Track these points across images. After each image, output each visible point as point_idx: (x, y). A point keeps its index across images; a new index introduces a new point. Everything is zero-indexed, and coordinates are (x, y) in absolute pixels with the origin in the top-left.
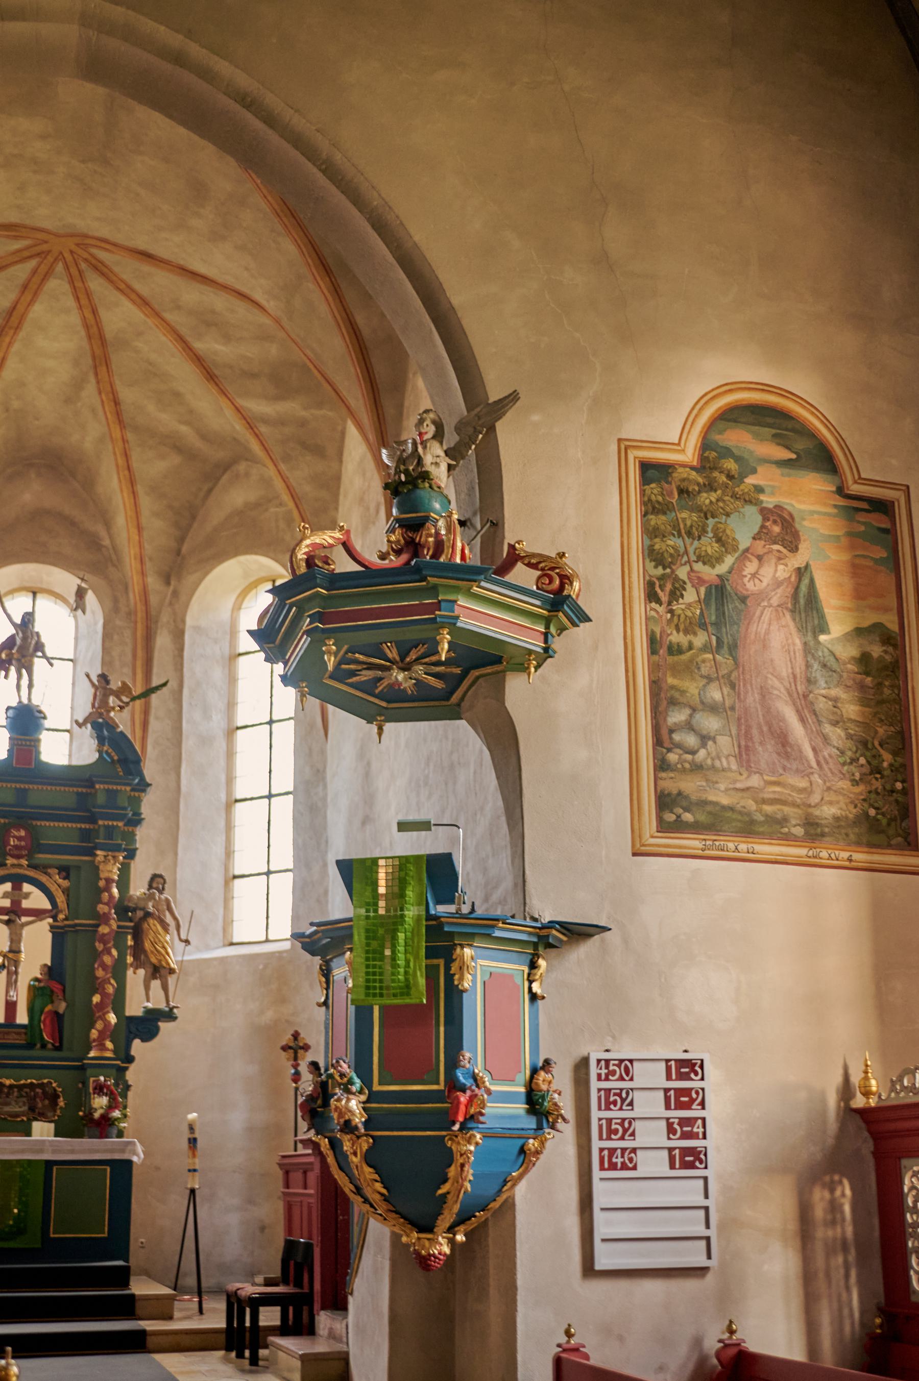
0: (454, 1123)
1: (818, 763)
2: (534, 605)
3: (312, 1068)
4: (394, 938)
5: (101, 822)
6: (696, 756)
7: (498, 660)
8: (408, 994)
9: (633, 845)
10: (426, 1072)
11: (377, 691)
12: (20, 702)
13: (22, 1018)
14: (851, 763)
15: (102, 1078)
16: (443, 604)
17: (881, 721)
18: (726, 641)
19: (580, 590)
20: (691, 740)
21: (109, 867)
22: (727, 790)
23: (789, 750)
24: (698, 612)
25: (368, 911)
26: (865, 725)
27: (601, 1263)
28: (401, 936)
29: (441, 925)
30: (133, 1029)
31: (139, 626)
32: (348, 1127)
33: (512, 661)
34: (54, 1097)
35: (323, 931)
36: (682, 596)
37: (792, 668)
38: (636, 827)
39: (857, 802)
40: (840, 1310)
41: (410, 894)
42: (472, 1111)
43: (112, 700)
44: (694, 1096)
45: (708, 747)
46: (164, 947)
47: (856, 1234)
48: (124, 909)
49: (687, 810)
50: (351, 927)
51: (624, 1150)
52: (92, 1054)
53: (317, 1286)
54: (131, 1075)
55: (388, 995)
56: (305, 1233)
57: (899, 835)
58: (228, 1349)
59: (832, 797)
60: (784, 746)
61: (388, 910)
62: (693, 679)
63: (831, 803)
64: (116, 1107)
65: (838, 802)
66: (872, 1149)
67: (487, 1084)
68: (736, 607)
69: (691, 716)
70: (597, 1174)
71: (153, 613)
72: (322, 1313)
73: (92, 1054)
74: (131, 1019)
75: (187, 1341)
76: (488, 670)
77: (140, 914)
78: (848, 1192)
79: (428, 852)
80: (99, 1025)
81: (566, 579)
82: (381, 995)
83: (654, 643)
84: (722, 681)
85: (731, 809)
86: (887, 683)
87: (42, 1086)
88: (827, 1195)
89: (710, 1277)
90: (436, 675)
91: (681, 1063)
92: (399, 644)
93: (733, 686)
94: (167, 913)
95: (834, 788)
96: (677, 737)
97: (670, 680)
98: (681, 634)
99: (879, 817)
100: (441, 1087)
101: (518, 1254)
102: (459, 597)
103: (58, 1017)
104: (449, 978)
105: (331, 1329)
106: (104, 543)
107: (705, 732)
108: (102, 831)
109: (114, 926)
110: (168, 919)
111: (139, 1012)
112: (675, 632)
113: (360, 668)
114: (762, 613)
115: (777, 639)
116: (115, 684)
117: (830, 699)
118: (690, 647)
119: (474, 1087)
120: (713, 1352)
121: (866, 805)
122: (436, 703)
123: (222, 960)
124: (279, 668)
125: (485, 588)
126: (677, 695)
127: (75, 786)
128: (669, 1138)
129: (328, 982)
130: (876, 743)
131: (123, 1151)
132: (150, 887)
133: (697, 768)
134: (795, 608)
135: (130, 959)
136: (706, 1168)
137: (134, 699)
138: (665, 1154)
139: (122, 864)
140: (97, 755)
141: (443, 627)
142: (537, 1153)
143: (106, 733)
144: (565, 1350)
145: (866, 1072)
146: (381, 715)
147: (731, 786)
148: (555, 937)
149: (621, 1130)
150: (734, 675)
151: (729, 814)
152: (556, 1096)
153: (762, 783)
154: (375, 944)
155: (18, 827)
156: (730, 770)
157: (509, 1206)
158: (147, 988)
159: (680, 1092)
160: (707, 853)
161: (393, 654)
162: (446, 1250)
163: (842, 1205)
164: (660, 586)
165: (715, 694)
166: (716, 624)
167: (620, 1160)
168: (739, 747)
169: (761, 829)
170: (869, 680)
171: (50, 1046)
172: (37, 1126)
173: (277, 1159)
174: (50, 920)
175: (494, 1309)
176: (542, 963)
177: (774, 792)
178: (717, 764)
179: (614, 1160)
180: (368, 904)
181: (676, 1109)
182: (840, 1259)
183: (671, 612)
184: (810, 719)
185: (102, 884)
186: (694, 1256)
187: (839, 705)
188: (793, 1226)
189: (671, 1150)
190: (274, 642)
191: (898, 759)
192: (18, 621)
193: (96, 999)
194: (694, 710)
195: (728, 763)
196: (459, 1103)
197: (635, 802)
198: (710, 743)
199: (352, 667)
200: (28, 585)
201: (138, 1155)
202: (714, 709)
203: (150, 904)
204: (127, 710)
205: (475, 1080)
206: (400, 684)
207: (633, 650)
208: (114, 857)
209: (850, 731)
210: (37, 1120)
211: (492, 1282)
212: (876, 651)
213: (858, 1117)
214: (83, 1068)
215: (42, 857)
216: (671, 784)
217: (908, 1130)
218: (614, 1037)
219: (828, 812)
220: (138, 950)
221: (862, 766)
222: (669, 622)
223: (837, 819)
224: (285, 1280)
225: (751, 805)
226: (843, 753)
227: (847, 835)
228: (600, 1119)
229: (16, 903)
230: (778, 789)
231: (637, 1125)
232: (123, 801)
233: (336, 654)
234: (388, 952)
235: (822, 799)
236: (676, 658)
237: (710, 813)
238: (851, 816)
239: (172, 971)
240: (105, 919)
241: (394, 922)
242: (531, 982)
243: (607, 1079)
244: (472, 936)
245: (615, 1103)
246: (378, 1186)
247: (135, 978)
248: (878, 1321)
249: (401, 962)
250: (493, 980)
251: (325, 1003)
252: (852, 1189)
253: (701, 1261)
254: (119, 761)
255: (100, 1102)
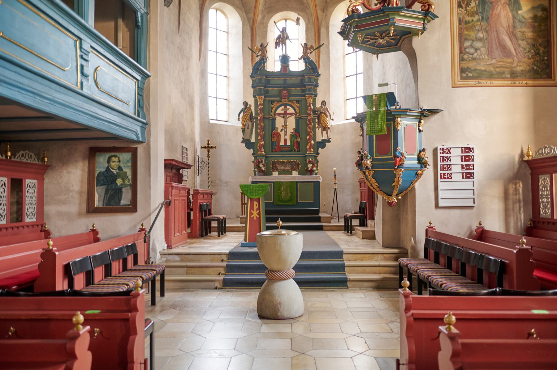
0: (396, 167)
1: (516, 53)
2: (419, 15)
3: (359, 153)
4: (378, 116)
5: (307, 87)
6: (473, 56)
7: (410, 33)
8: (382, 132)
9: (452, 84)
10: (387, 152)
11: (375, 45)
12: (283, 54)
13: (289, 143)
14: (528, 52)
15: (310, 159)
16: (391, 19)
17: (540, 37)
18: (485, 17)
19: (434, 8)
20: (472, 51)
21: (310, 100)
22: (484, 65)
23: (506, 50)
24: (475, 9)
25: (370, 110)
26: (534, 40)
27: (440, 205)
28: (380, 116)
29: (391, 112)
30: (319, 146)
31: (316, 26)
32: (367, 168)
33: (414, 33)
34: (298, 164)
35: (359, 116)
36: (470, 5)
37: (508, 23)
38: (453, 79)
39: (530, 65)
40: (517, 219)
41: (382, 104)
42: (401, 163)
43: (308, 51)
44: (470, 158)
45: (478, 52)
46: (326, 122)
47: (523, 198)
48: (315, 112)
49: (470, 72)
50: (366, 114)
51: (448, 173)
52: (308, 153)
53: (368, 214)
54: (319, 158)
55: (376, 132)
56: (365, 200)
57: (545, 74)
58: (345, 231)
59: (521, 64)
60: (504, 49)
61: (376, 109)
62: (473, 31)
63: (520, 66)
64: (314, 167)
65: (523, 65)
66: (530, 172)
67: (405, 155)
68: (489, 6)
69: (472, 43)
70: (439, 180)
71: (320, 22)
72: (369, 220)
73: (308, 153)
74: (318, 142)
75: (334, 228)
76: (407, 36)
77: (319, 112)
78: (521, 185)
79: (387, 92)
80: (309, 144)
81: (430, 6)
82: (374, 132)
83: (460, 21)
84: (483, 31)
85: (485, 71)
86: (543, 24)
87: (295, 162)
88: (514, 186)
89: (474, 209)
90: (392, 39)
91: (466, 148)
92: (379, 32)
93: (487, 32)
94: (327, 112)
95: (522, 61)
96: (467, 50)
97: (465, 32)
98: (469, 17)
99: (538, 69)
100: (392, 157)
101: (416, 202)
102: (396, 16)
103: (298, 143)
104: (394, 127)
105: (371, 225)
106: (304, 2)
107: (476, 48)
108: (307, 89)
109: (312, 117)
110: (327, 113)
111: (320, 140)
112: (467, 17)
113: (369, 39)
114: (498, 7)
115: (503, 14)
116: (309, 46)
117: (521, 32)
118: (472, 21)
119: (401, 157)
120: (474, 230)
121: (533, 66)
122: (394, 47)
123: (344, 124)
124: (347, 42)
125: (404, 13)
126: (467, 37)
127: (300, 77)
128: (462, 170)
129: (362, 129)
130: (538, 45)
131: (317, 179)
132: (322, 104)
133: (474, 59)
134: (510, 3)
135: (317, 126)
136: (474, 178)
137: (314, 50)
138: (461, 174)
139: (313, 98)
140: (305, 67)
141: (391, 26)
142: (421, 174)
143: (307, 61)
144: (429, 228)
145: (528, 149)
146: (377, 52)
147: (485, 64)
148: (426, 113)
149: (447, 168)
150: (487, 28)
151: (484, 73)
152: (426, 158)
153: (496, 62)
154: (372, 118)
155: (284, 90)
156: (485, 59)
157: (414, 189)
158: (322, 133)
159: (466, 157)
160: (476, 85)
161: (378, 35)
162: (396, 201)
163: (519, 189)
164: (463, 3)
165: (481, 35)
166: (482, 13)
167: (447, 176)
168: (488, 51)
169: (495, 76)
170: (536, 24)
171: (296, 151)
172: (293, 172)
173: (358, 180)
174: (295, 116)
175: (410, 217)
176: (422, 121)
177: (500, 64)
178: (481, 57)
179: (445, 176)
180: (370, 108)
181: (464, 161)
182: (518, 205)
183: (466, 10)
184: (514, 39)
185: (308, 104)
186: (470, 203)
187: (525, 34)
188: (502, 195)
189: (463, 173)
190: (345, 35)
191: (546, 49)
192: (281, 30)
193: (308, 137)
194: (473, 41)
195: (484, 57)
196: (397, 161)
197: (453, 71)
198: (478, 51)
199: (367, 39)
200: (284, 18)
201: (321, 180)
202: (480, 40)
203: (322, 110)
204: (313, 53)
205: (402, 154)
206: (381, 43)
207: (453, 24)
208: (311, 97)
209: (529, 42)
210: (293, 171)
211: (409, 210)
212: (540, 14)
213: (526, 163)
214: (305, 156)
215: (291, 98)
216: (465, 65)
217: (544, 166)
218: (445, 142)
219: (519, 69)
220: (319, 123)
221: (532, 53)
222: (466, 14)
223: (522, 71)
224: (360, 212)
225: (492, 69)
226: (525, 49)
227: (526, 76)
228: (441, 165)
229: (285, 112)
230: (501, 63)
231: (452, 166)
232: (313, 80)
233: (361, 37)
234: (376, 121)
235: (517, 65)
236: (467, 25)
237: (477, 73)
238: (527, 69)
239: (329, 128)
240: (309, 115)
241: (378, 112)
242: (419, 127)
243: (443, 153)
244: (401, 115)
245: (445, 160)
246: (376, 184)
247: (319, 131)
248: (529, 223)
249: (380, 123)
250: (407, 128)
251: (362, 135)
252: (523, 184)
253: (472, 204)
254: (311, 68)
255: (310, 166)
